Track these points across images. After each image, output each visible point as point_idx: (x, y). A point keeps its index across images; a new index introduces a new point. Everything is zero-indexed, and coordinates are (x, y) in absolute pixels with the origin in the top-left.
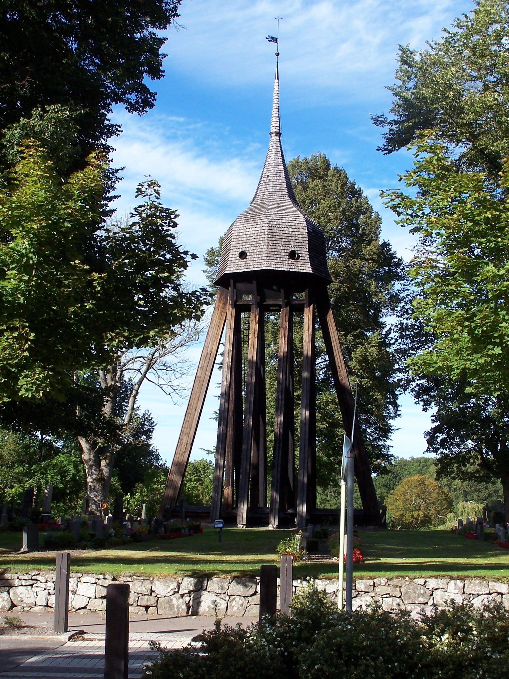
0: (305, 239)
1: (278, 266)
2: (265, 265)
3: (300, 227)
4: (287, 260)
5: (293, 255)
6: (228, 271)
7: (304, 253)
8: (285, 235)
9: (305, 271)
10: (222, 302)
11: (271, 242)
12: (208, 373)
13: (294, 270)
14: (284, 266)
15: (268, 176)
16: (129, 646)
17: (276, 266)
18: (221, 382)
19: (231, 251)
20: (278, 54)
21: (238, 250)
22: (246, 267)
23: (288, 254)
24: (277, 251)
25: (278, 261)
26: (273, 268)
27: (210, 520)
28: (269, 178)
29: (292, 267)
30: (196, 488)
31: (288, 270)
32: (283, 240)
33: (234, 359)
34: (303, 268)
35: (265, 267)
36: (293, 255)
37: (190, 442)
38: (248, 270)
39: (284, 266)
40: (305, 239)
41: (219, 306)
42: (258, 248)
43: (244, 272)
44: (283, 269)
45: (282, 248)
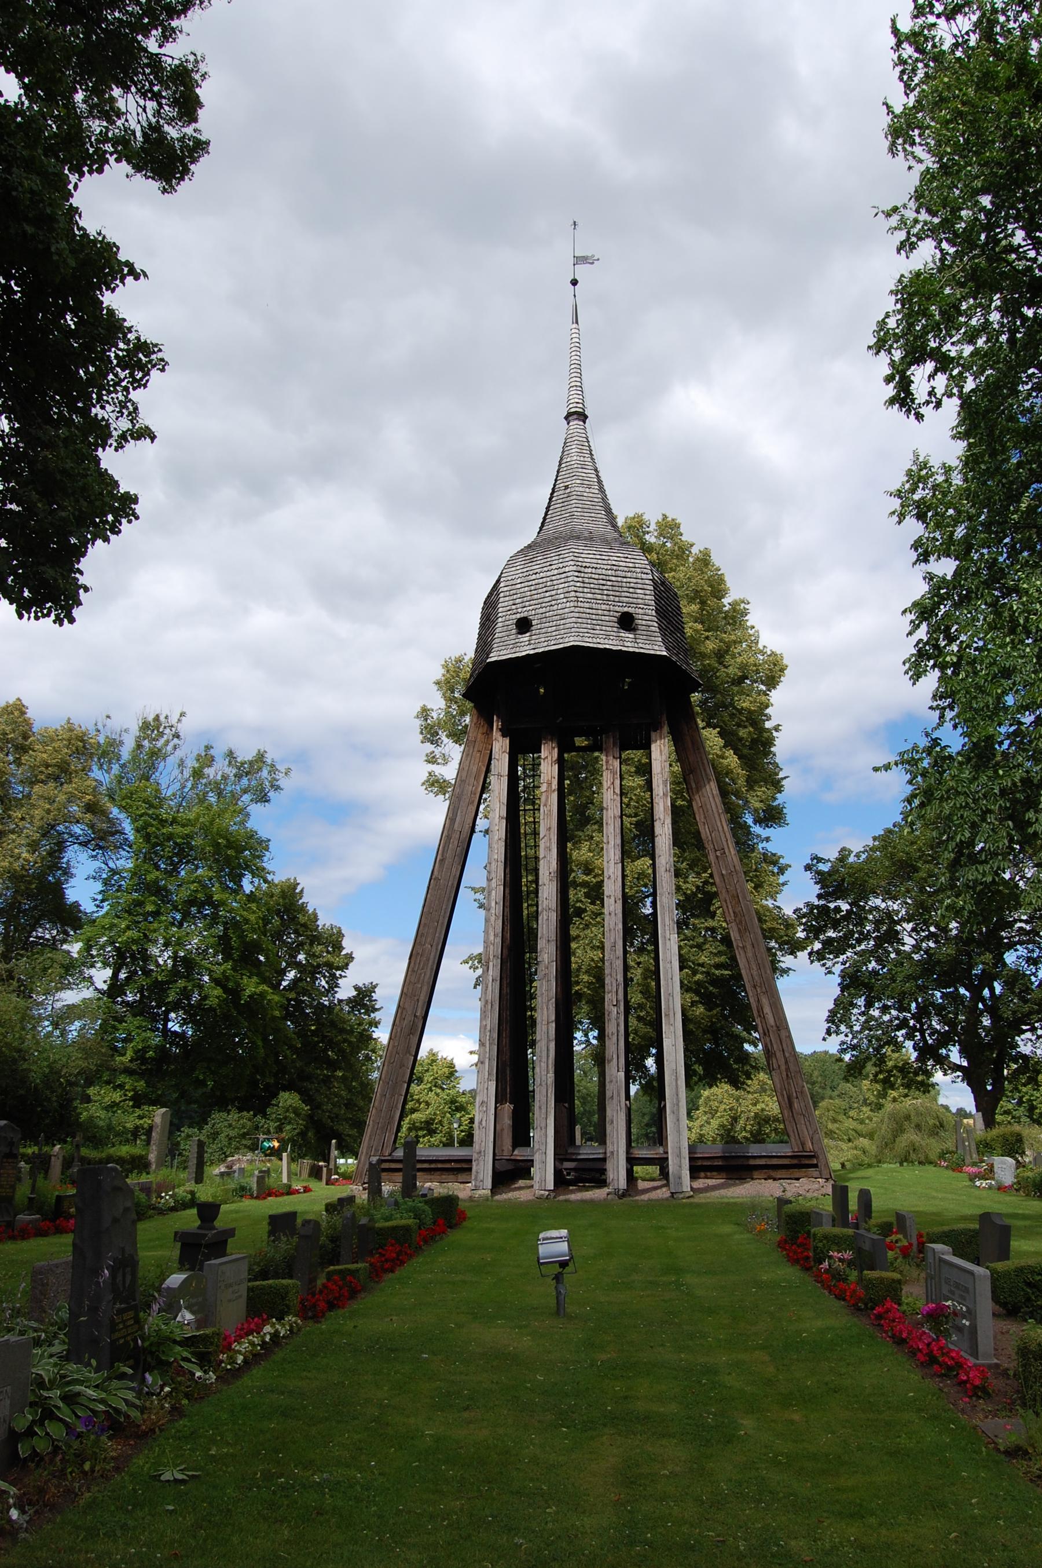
0: (648, 592)
1: (598, 640)
2: (572, 639)
3: (638, 570)
4: (615, 629)
5: (627, 622)
6: (494, 657)
7: (647, 615)
8: (609, 583)
9: (652, 652)
10: (481, 731)
11: (581, 595)
12: (426, 989)
13: (631, 650)
14: (611, 642)
15: (567, 487)
16: (873, 1208)
17: (595, 640)
18: (484, 884)
19: (500, 620)
20: (574, 282)
21: (514, 617)
22: (532, 646)
23: (615, 619)
24: (594, 611)
25: (597, 632)
26: (588, 645)
27: (787, 1208)
28: (568, 490)
29: (626, 644)
31: (620, 648)
32: (606, 592)
33: (507, 894)
34: (647, 646)
35: (571, 641)
36: (627, 622)
37: (420, 1013)
38: (536, 651)
39: (611, 642)
40: (648, 592)
41: (476, 738)
42: (555, 607)
43: (528, 655)
44: (608, 647)
45: (604, 607)
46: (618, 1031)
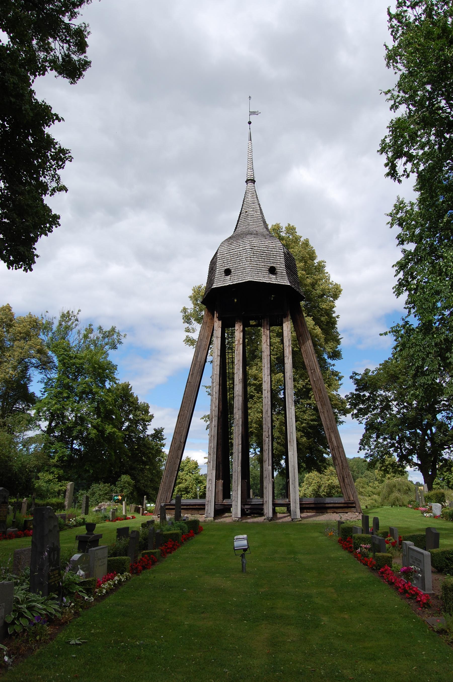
0: (282, 258)
1: (260, 279)
2: (249, 278)
3: (278, 248)
4: (267, 274)
5: (272, 270)
6: (215, 286)
7: (281, 267)
8: (265, 254)
9: (283, 284)
10: (209, 318)
11: (253, 259)
12: (185, 430)
13: (274, 283)
14: (265, 279)
15: (246, 212)
17: (258, 278)
18: (210, 385)
20: (250, 123)
21: (223, 268)
22: (231, 281)
23: (268, 269)
24: (258, 266)
25: (260, 275)
26: (256, 280)
27: (342, 525)
28: (247, 213)
29: (272, 280)
30: (449, 194)
31: (269, 282)
32: (263, 258)
34: (281, 281)
35: (248, 279)
36: (272, 270)
37: (182, 441)
38: (233, 283)
39: (265, 279)
40: (282, 258)
41: (207, 321)
42: (241, 264)
43: (230, 285)
44: (264, 281)
45: (262, 264)
46: (269, 449)
